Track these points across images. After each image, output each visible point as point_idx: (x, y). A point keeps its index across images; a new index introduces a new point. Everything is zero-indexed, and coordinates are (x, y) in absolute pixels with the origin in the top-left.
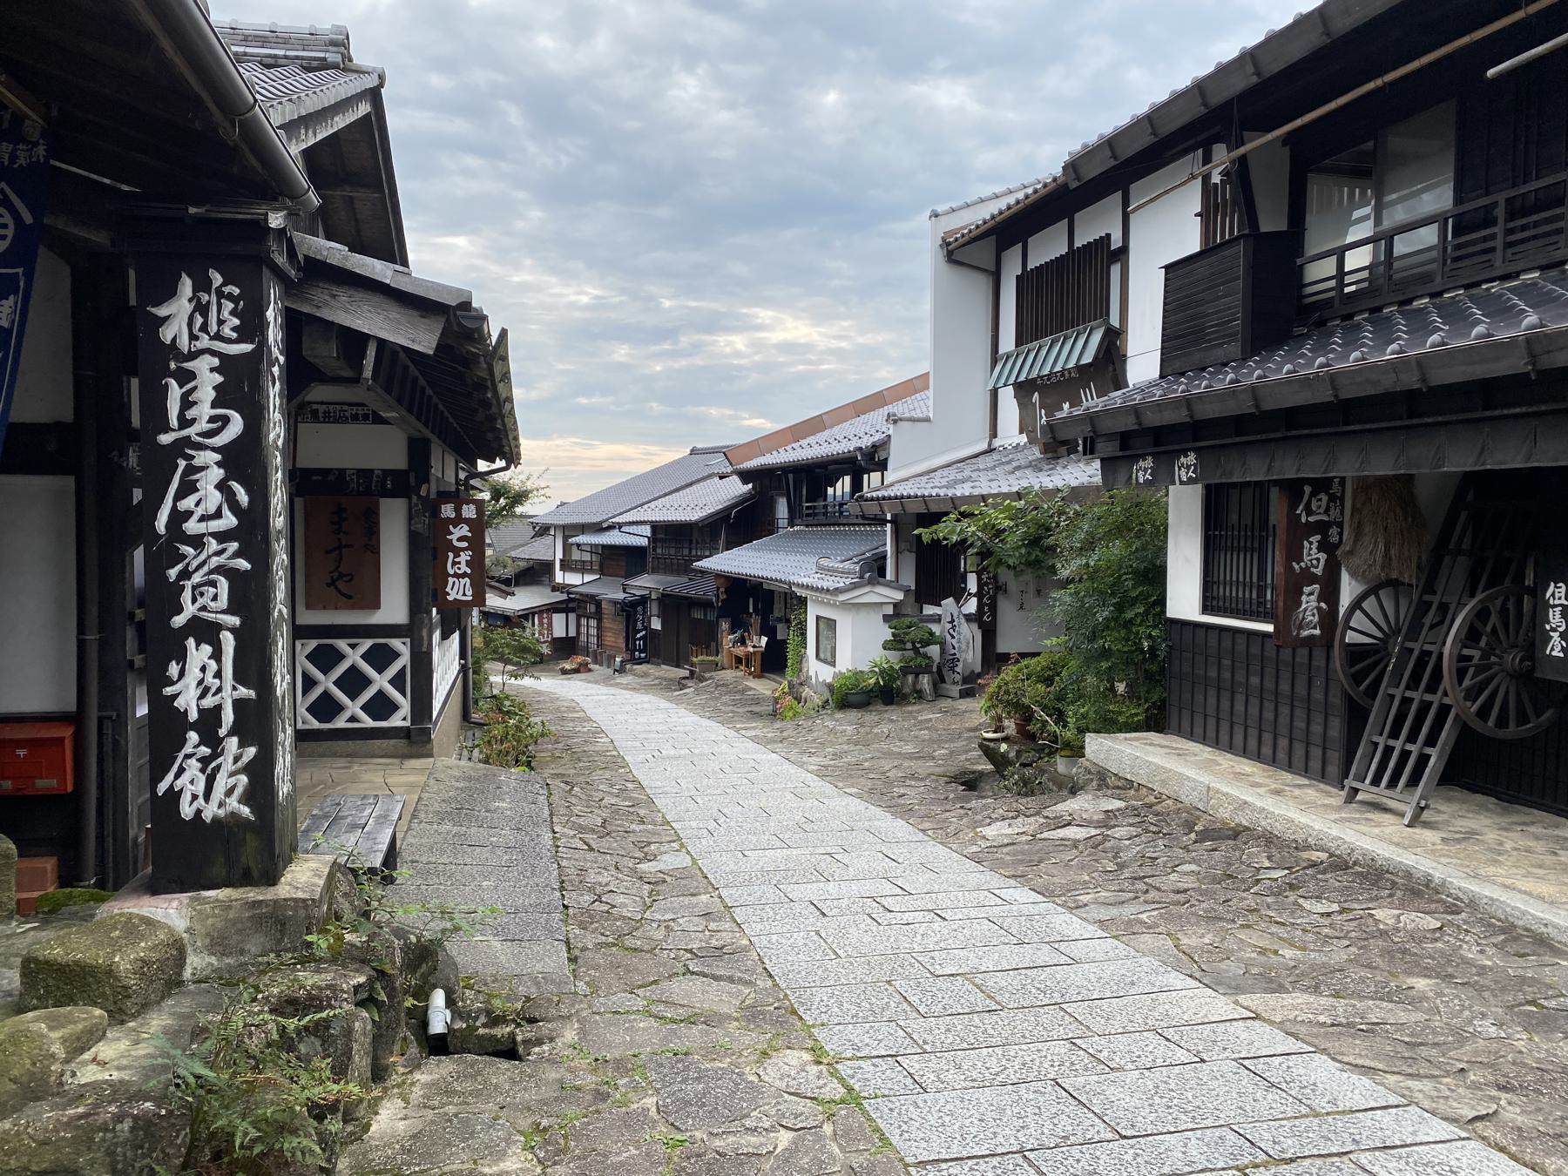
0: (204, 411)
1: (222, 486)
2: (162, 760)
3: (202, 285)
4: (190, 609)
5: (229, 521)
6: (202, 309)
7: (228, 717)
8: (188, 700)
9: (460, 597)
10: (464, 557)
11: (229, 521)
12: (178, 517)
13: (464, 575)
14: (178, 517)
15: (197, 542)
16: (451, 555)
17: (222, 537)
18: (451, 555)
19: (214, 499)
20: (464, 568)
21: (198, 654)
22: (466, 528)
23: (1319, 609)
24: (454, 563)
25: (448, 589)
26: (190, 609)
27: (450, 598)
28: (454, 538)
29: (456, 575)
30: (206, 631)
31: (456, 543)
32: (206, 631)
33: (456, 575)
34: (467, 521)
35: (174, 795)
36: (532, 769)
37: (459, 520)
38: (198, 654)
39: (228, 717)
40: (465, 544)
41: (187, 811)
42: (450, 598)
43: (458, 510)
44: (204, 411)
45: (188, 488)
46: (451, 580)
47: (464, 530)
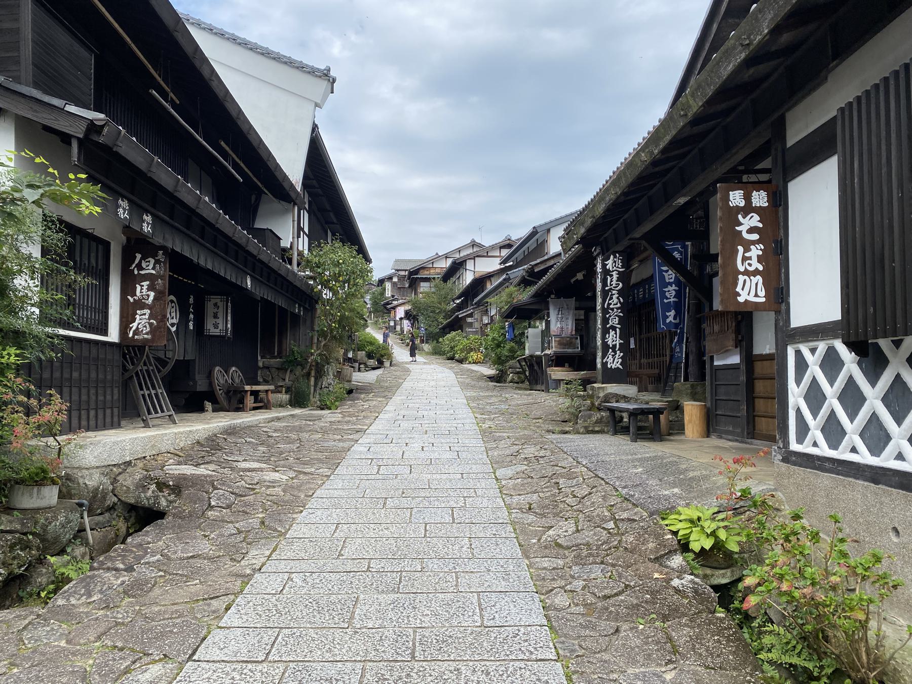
0: (614, 283)
1: (618, 298)
2: (604, 355)
3: (615, 257)
4: (611, 323)
5: (619, 305)
6: (615, 262)
7: (618, 346)
8: (610, 343)
9: (752, 298)
10: (755, 252)
11: (619, 305)
12: (609, 304)
13: (756, 273)
14: (609, 304)
15: (612, 309)
16: (740, 249)
17: (618, 309)
18: (740, 249)
19: (615, 300)
20: (756, 265)
21: (612, 333)
22: (756, 217)
23: (151, 325)
24: (744, 259)
25: (739, 289)
26: (611, 323)
27: (741, 299)
28: (743, 229)
29: (746, 273)
30: (614, 328)
31: (745, 235)
32: (614, 328)
33: (746, 273)
34: (758, 210)
35: (607, 362)
36: (874, 555)
37: (748, 209)
38: (612, 333)
39: (618, 346)
40: (755, 237)
41: (609, 366)
42: (741, 299)
43: (748, 198)
44: (614, 283)
45: (611, 298)
46: (741, 278)
47: (754, 220)
